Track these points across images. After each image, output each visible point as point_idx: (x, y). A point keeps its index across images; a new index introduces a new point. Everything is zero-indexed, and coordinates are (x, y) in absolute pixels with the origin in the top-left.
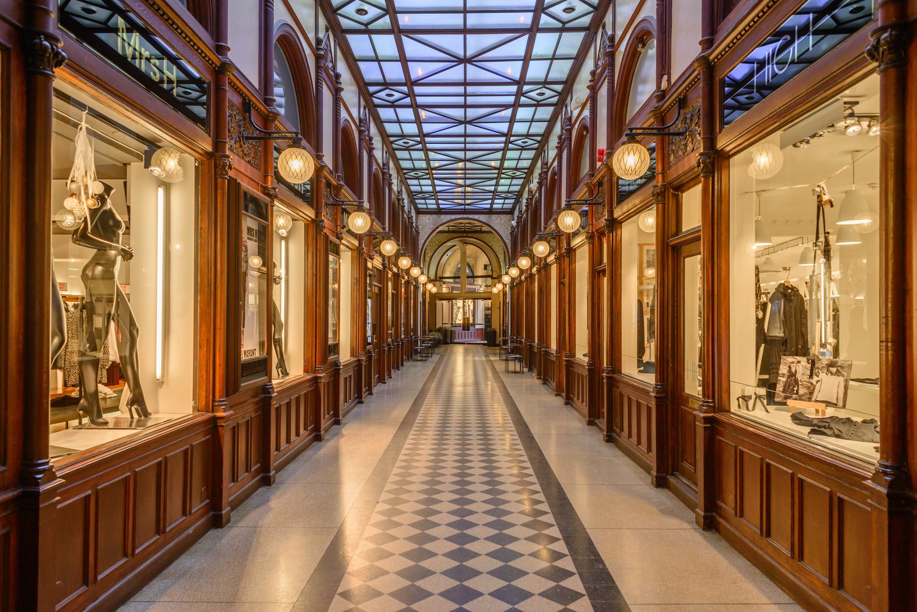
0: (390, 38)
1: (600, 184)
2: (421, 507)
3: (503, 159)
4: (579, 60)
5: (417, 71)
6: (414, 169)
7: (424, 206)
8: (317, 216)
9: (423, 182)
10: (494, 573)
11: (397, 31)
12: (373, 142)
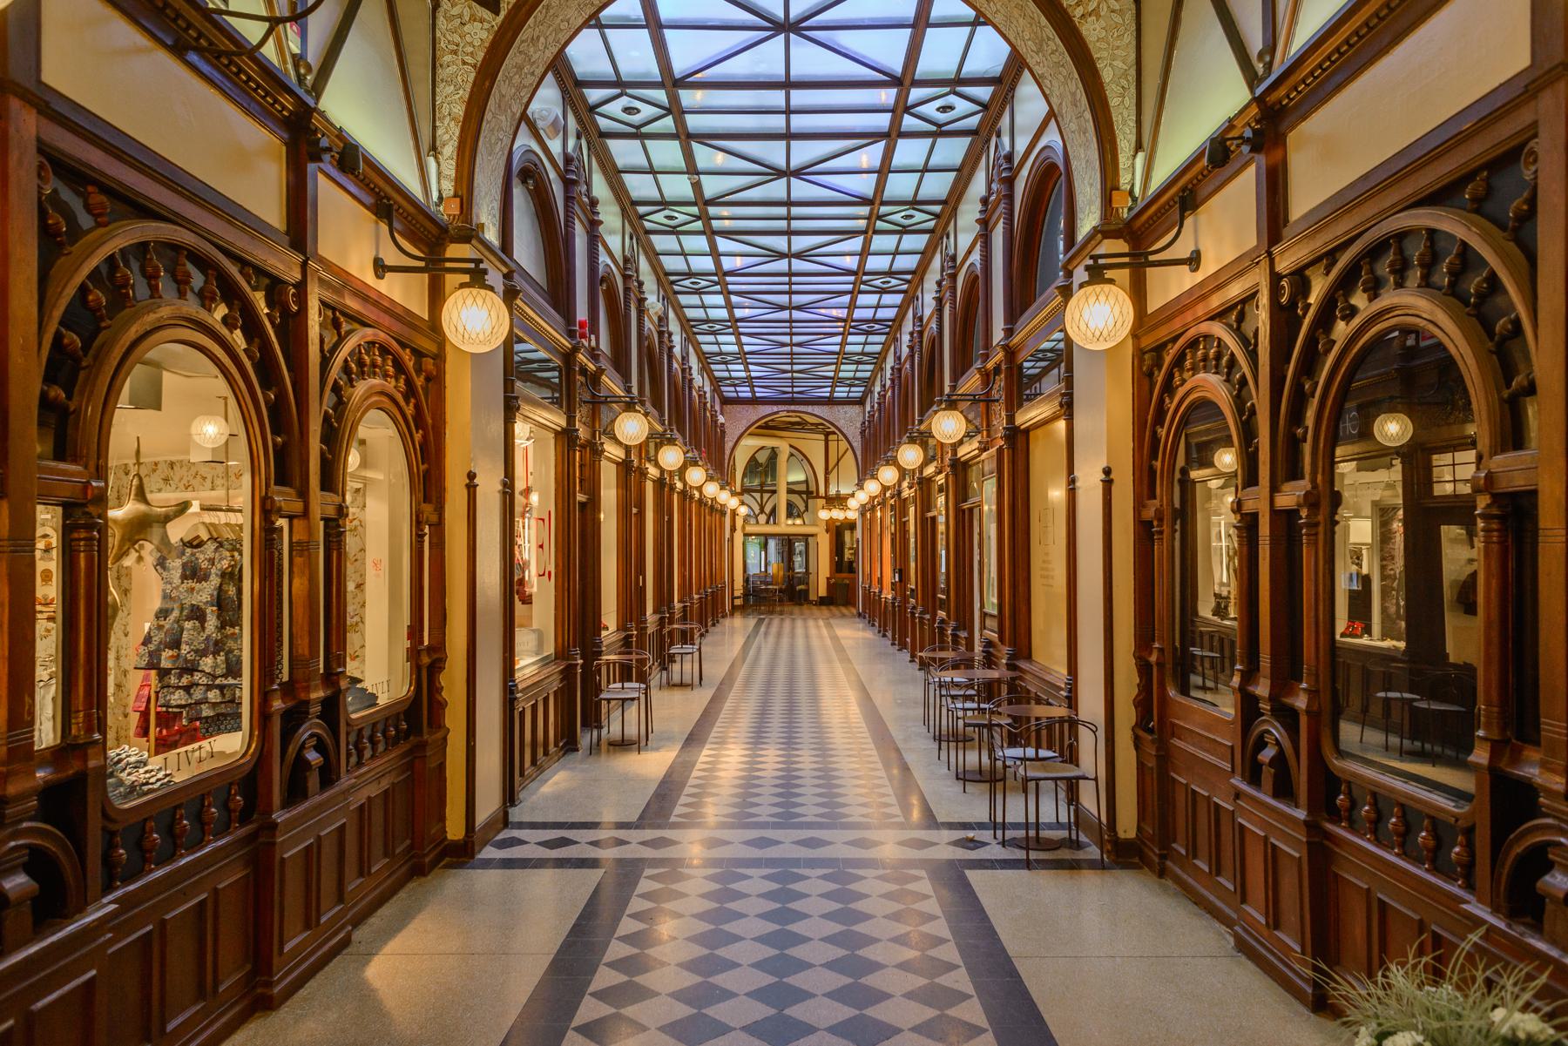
0: (675, 145)
1: (997, 370)
2: (704, 927)
3: (852, 306)
8: (568, 423)
9: (708, 299)
10: (837, 995)
12: (599, 208)
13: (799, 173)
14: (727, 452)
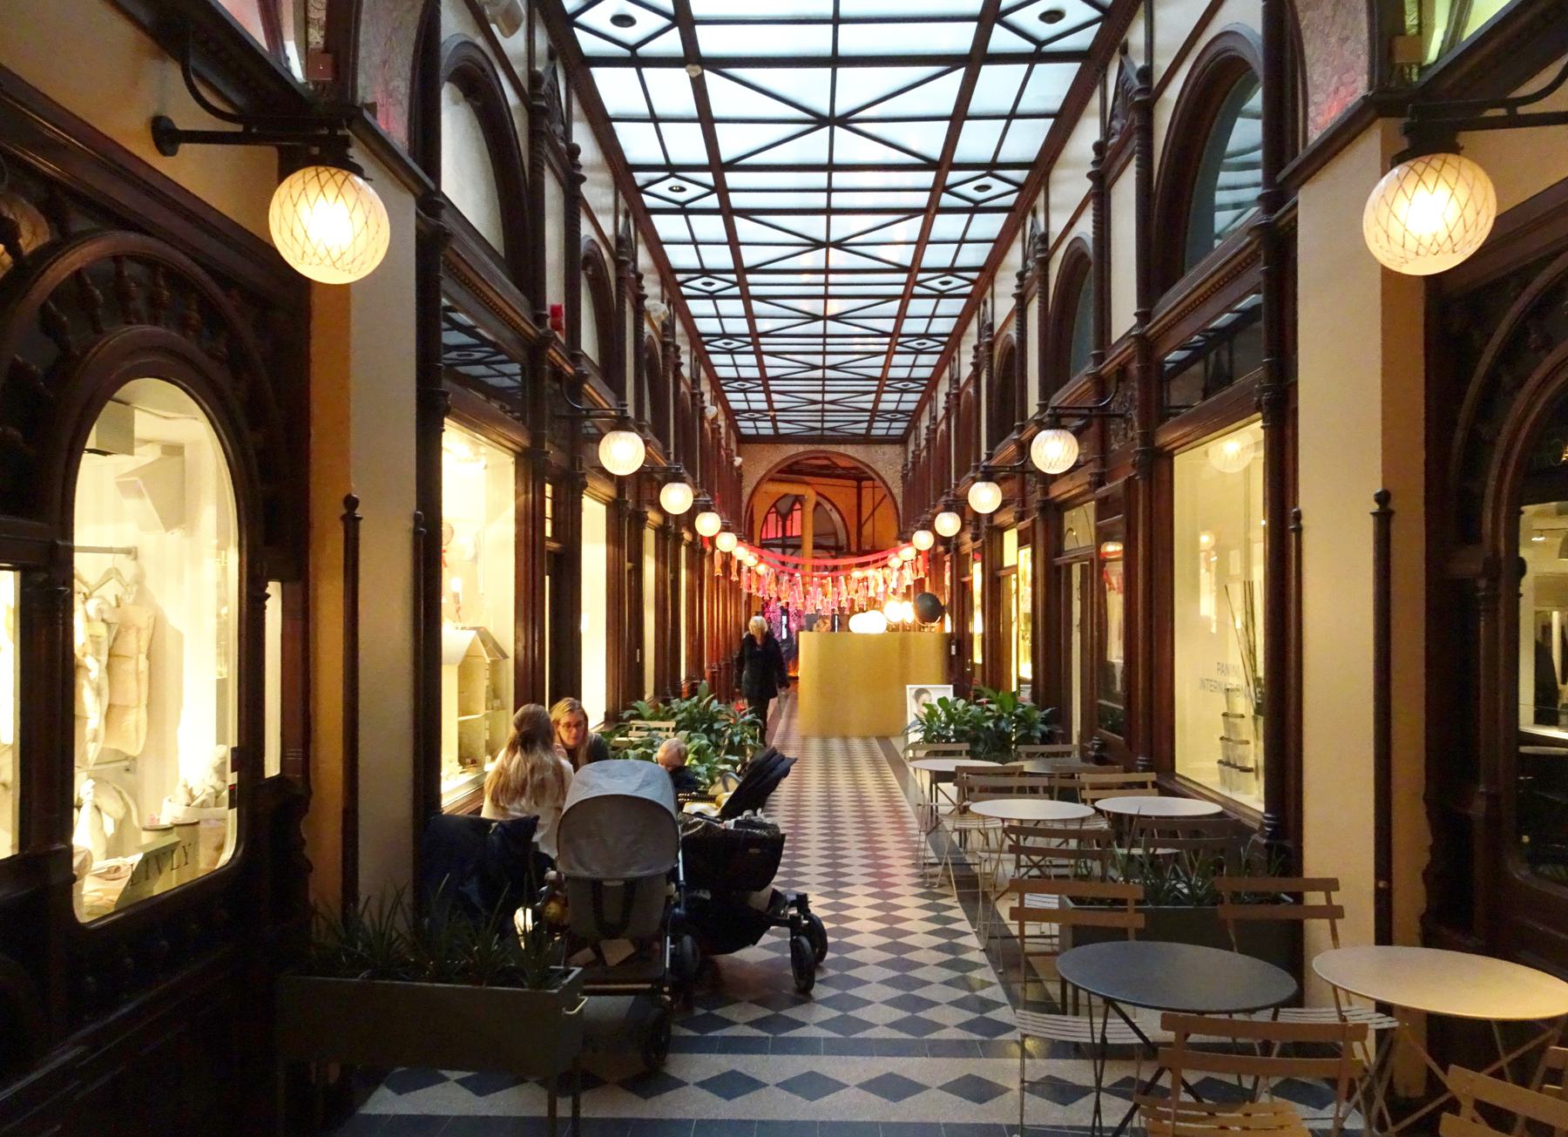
3: (901, 316)
4: (1064, 120)
5: (732, 142)
6: (724, 335)
7: (753, 432)
9: (740, 359)
11: (691, 57)
12: (644, 283)
13: (845, 121)
14: (745, 499)
